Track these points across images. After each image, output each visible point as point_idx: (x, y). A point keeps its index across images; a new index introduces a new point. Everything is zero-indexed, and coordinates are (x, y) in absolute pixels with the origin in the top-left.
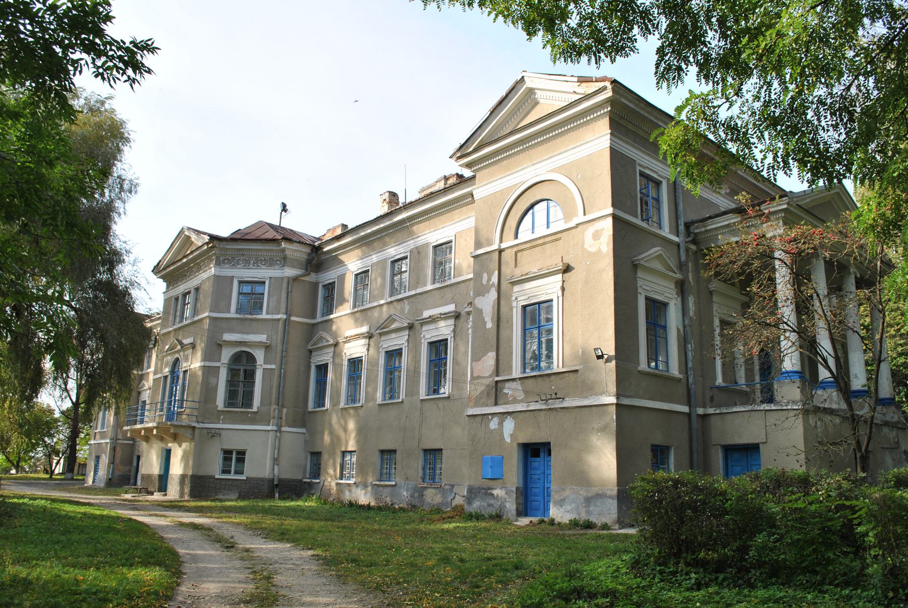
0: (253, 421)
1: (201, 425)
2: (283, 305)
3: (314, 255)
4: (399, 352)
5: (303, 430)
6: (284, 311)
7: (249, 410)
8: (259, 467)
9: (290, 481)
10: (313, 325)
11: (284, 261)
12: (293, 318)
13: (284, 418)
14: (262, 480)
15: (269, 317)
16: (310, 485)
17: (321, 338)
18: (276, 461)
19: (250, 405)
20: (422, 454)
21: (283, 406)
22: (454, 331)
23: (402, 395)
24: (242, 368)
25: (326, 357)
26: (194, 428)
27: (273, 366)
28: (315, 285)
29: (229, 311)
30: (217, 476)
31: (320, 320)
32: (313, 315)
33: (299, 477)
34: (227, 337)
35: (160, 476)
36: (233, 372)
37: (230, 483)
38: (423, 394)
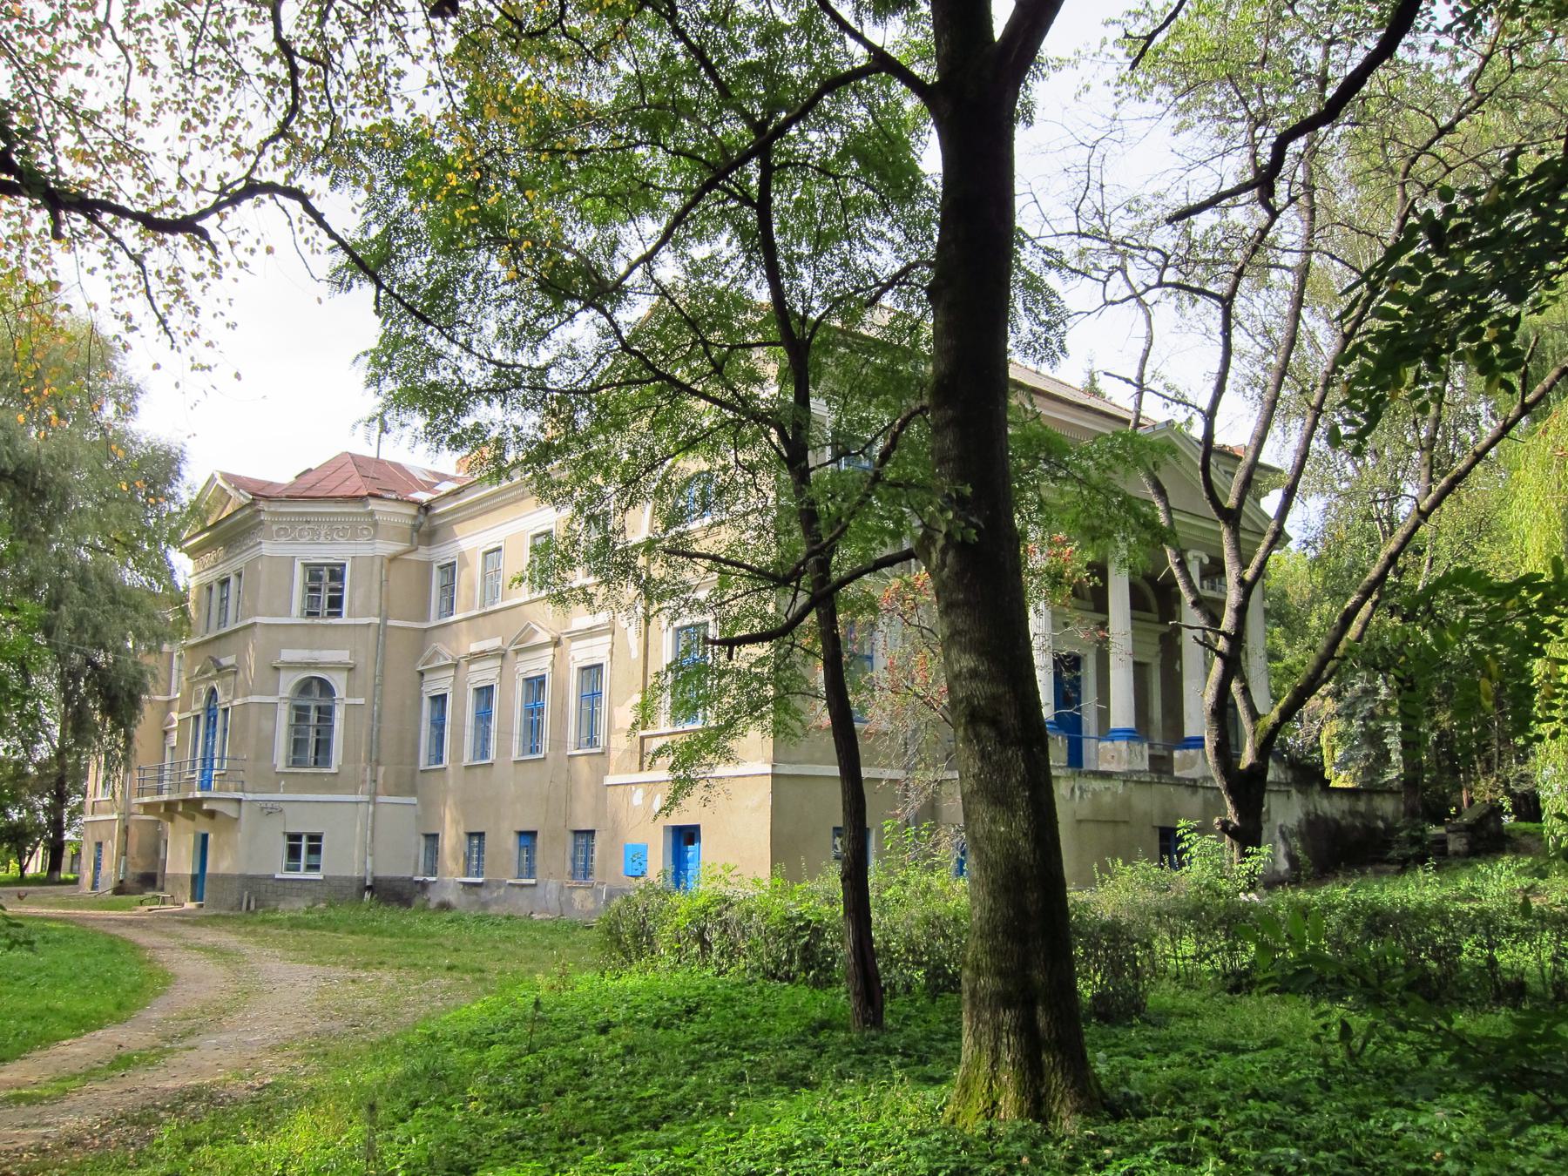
0: (331, 789)
1: (250, 796)
2: (375, 602)
3: (422, 518)
4: (540, 681)
5: (414, 800)
6: (377, 611)
7: (325, 770)
8: (345, 858)
9: (391, 880)
10: (426, 630)
11: (375, 527)
12: (391, 623)
13: (380, 781)
14: (350, 879)
15: (352, 621)
16: (424, 886)
17: (436, 653)
18: (371, 848)
19: (327, 763)
20: (570, 837)
21: (378, 763)
22: (500, 675)
23: (493, 755)
24: (313, 705)
25: (440, 683)
26: (239, 801)
27: (361, 701)
28: (427, 565)
29: (289, 614)
30: (278, 876)
31: (433, 623)
32: (425, 617)
33: (409, 875)
34: (288, 655)
35: (194, 878)
36: (301, 714)
37: (288, 885)
38: (516, 754)
